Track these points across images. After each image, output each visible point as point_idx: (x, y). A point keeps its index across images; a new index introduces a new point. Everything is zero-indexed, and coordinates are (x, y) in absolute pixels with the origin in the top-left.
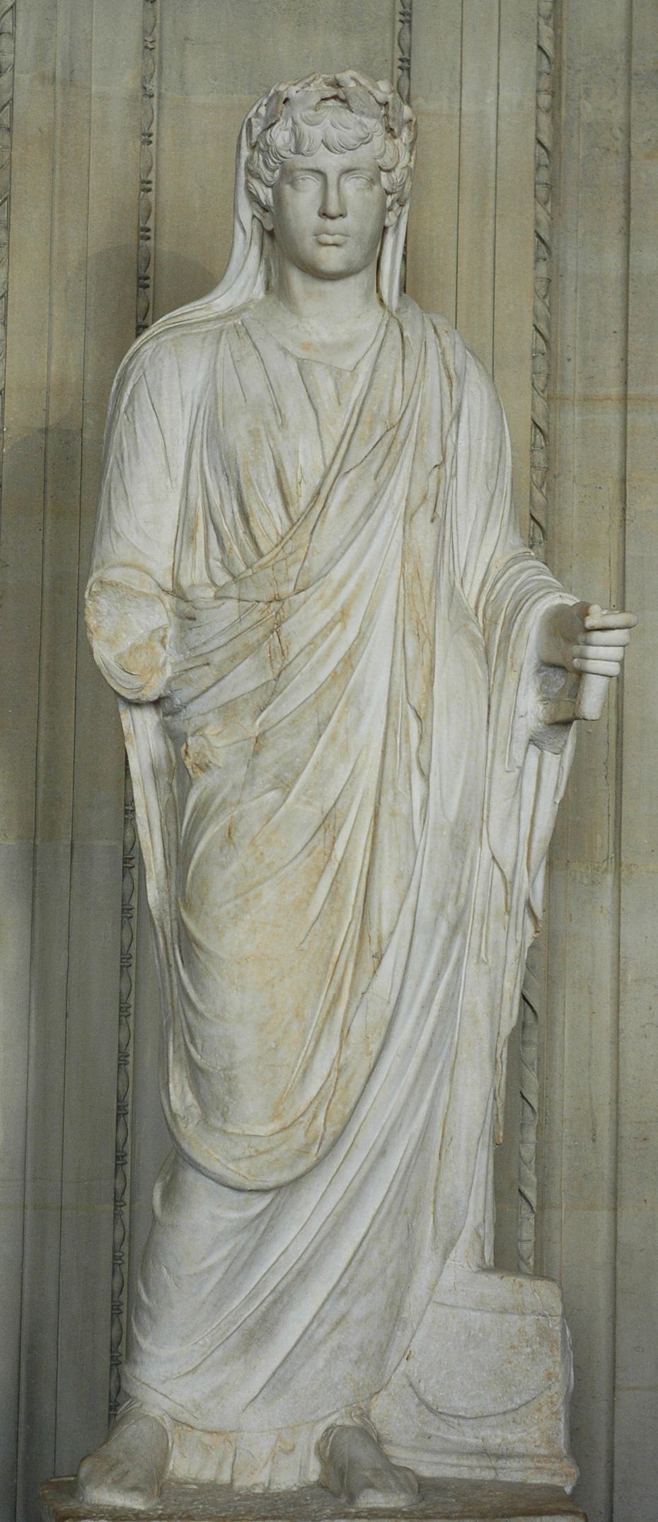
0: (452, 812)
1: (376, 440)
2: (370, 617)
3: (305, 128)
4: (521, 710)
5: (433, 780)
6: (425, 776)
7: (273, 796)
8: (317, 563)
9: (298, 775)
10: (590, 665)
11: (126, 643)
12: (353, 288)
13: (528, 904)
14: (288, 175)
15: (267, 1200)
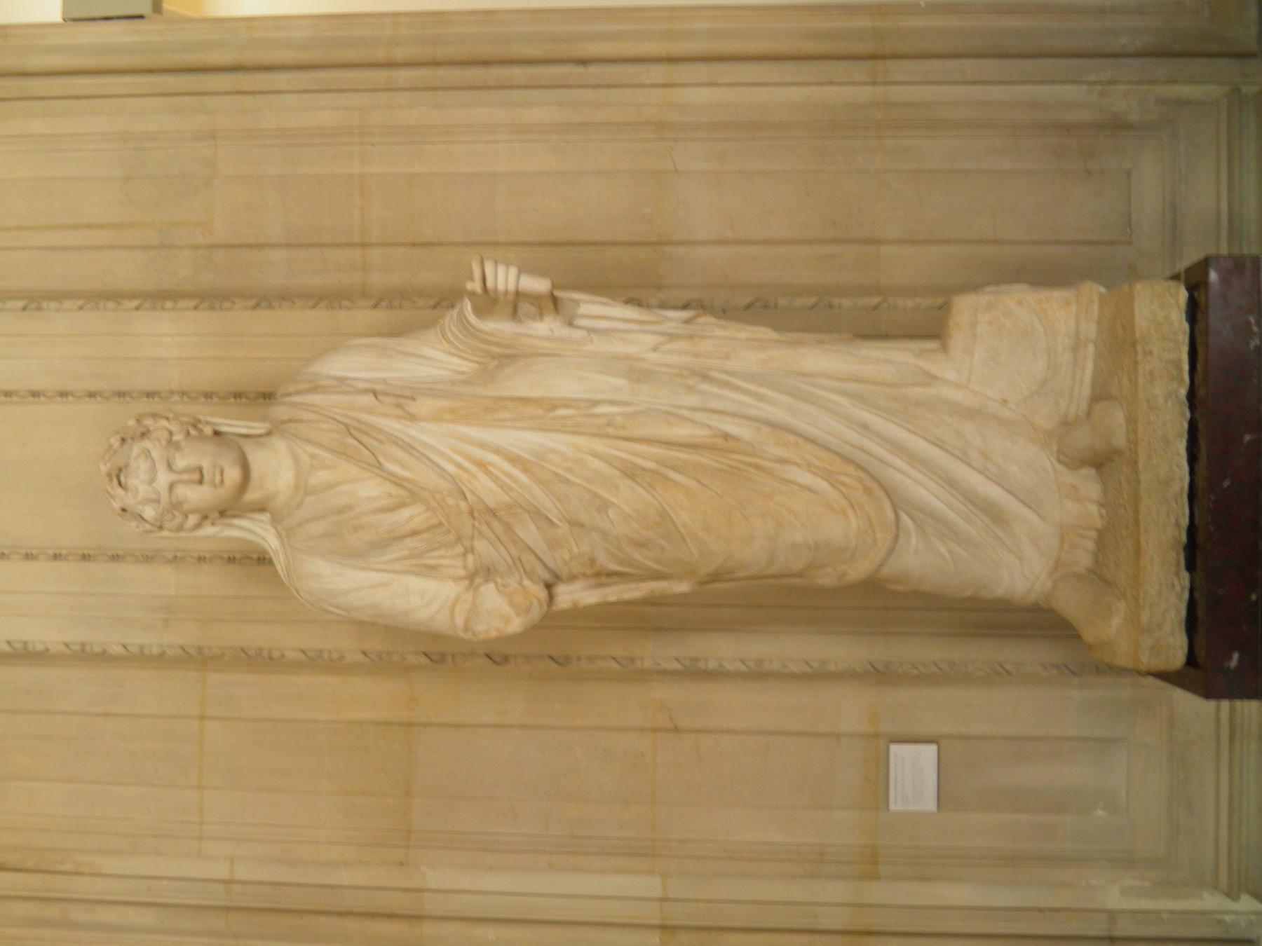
0: (620, 382)
1: (356, 442)
2: (483, 445)
3: (140, 497)
4: (548, 333)
5: (600, 396)
6: (595, 403)
7: (611, 513)
8: (444, 485)
9: (596, 495)
10: (511, 287)
11: (508, 610)
12: (257, 458)
13: (687, 322)
14: (176, 506)
15: (904, 517)
